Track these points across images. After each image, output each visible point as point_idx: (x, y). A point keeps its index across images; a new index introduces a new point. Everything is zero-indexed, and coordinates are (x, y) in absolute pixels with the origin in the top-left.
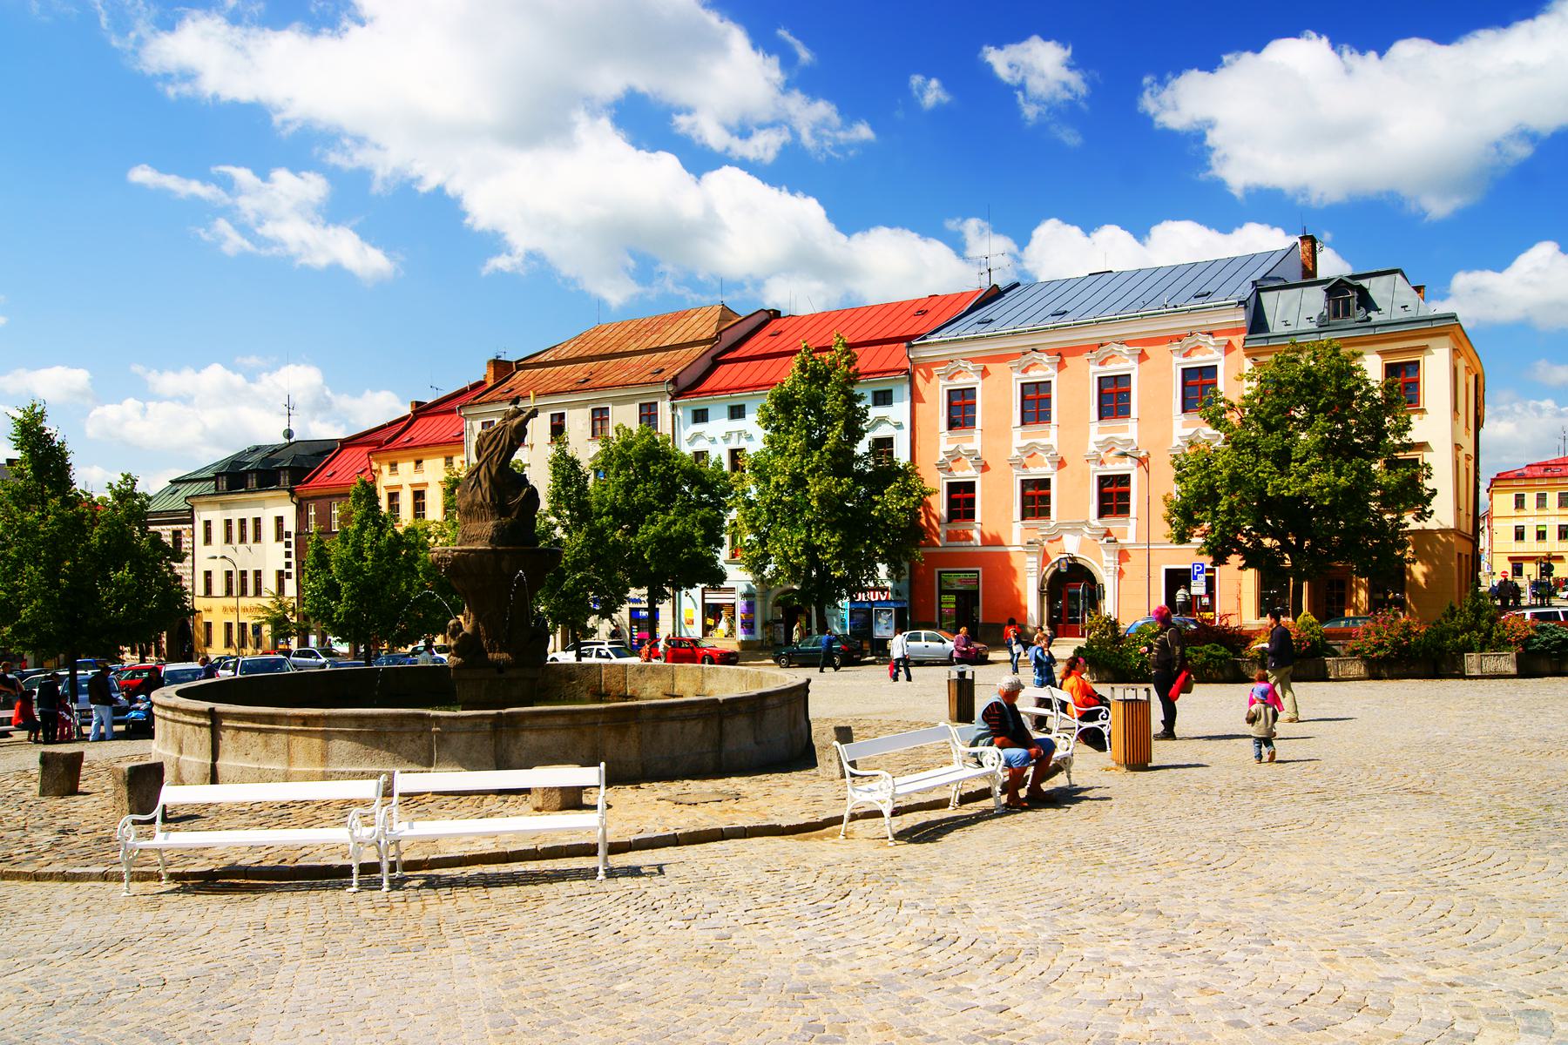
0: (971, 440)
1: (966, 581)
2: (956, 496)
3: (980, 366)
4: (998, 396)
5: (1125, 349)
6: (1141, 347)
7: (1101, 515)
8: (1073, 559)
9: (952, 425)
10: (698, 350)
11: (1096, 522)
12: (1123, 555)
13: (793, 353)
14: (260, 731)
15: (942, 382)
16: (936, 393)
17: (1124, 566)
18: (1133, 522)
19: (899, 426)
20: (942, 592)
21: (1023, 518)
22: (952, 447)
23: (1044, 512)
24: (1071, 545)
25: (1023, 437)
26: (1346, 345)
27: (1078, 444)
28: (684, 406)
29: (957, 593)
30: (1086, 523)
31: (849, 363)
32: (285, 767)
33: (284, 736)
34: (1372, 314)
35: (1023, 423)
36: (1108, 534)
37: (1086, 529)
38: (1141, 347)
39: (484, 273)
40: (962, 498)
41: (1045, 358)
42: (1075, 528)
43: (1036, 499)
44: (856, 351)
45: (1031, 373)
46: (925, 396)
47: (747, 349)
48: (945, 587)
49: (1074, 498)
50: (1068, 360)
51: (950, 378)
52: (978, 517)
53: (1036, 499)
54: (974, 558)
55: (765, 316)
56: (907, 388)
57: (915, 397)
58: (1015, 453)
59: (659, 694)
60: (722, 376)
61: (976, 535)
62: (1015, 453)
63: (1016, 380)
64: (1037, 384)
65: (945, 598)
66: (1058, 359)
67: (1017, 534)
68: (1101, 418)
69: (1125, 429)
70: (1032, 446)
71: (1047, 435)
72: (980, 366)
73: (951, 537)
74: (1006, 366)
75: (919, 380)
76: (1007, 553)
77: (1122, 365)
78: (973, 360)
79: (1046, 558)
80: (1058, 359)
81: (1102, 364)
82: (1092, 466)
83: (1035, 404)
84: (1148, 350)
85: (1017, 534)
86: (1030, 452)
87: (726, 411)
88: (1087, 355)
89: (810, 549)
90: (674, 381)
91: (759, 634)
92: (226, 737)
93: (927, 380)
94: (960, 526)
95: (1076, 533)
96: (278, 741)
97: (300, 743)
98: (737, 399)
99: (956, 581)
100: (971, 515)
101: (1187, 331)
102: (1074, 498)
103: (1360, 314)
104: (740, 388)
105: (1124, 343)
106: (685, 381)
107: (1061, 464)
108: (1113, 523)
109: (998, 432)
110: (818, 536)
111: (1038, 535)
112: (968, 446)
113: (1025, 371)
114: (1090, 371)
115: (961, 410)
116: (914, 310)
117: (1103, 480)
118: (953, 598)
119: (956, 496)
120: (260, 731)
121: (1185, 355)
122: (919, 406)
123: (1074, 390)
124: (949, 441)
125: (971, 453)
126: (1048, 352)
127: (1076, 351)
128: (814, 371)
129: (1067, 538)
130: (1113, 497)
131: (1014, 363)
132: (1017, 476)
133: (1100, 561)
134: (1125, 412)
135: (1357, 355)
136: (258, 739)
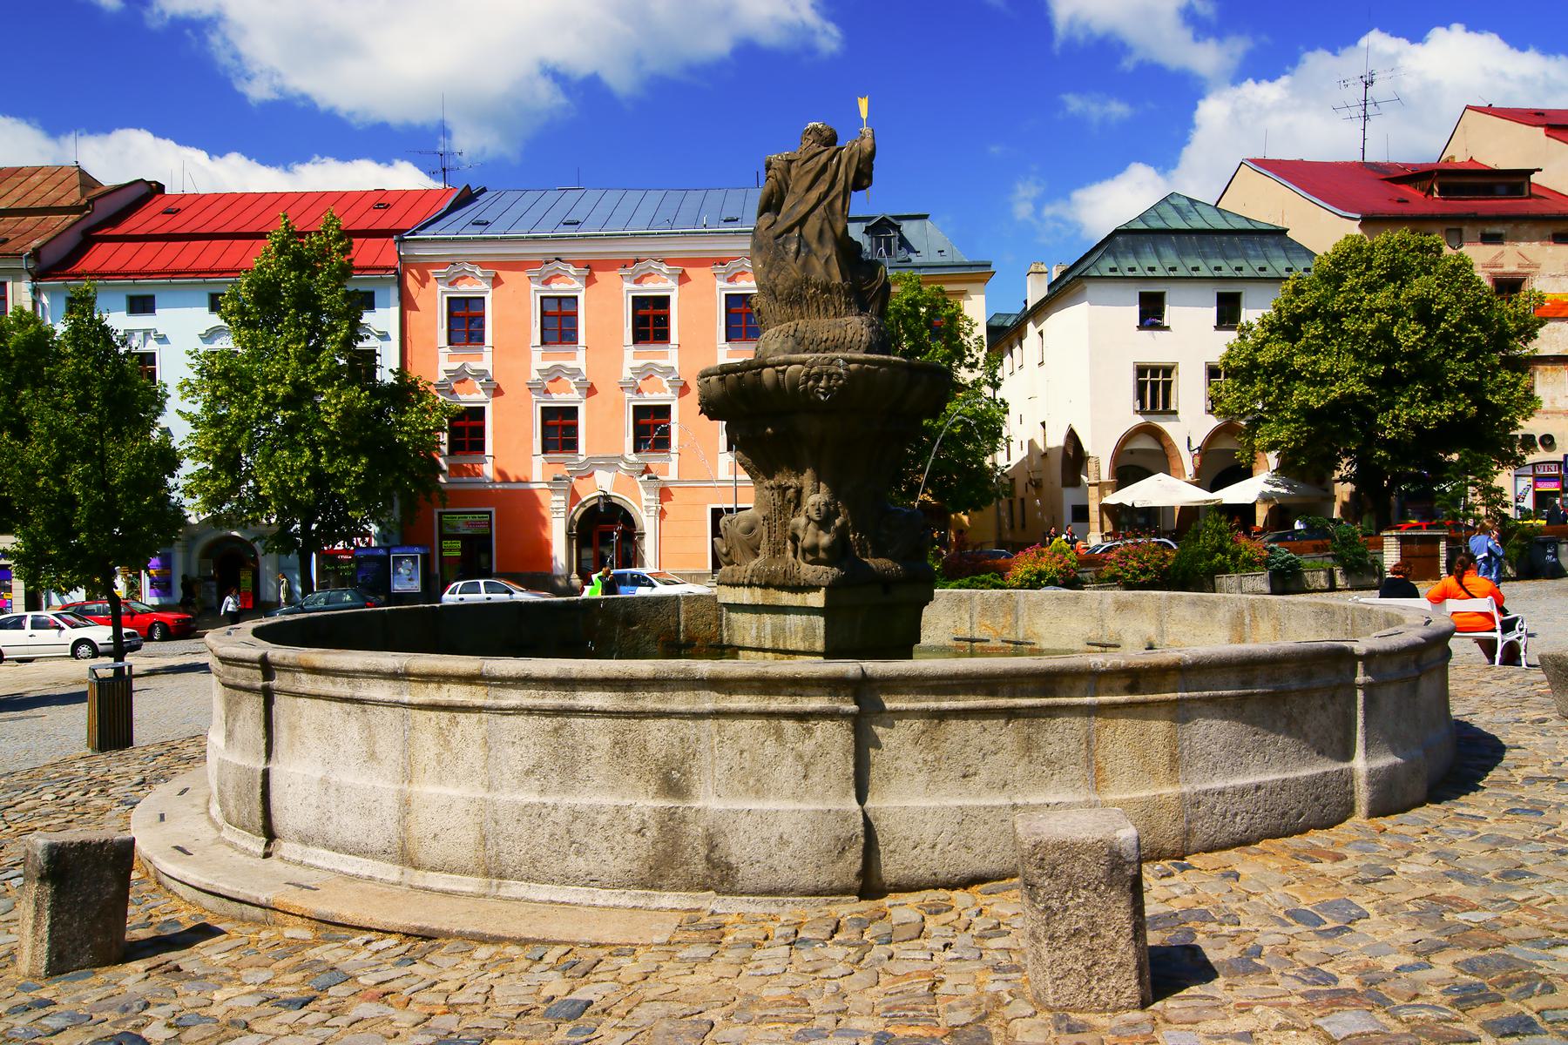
0: (665, 356)
1: (474, 524)
2: (550, 422)
3: (491, 272)
4: (513, 308)
5: (664, 268)
6: (590, 270)
7: (637, 450)
8: (607, 497)
9: (640, 336)
10: (58, 222)
11: (633, 458)
12: (665, 494)
13: (260, 236)
14: (1011, 714)
15: (441, 288)
16: (434, 300)
17: (666, 505)
18: (675, 458)
19: (384, 336)
20: (443, 537)
21: (544, 451)
22: (456, 365)
23: (570, 445)
24: (604, 482)
25: (544, 358)
26: (928, 283)
27: (610, 371)
28: (52, 292)
29: (465, 539)
30: (622, 458)
31: (345, 251)
32: (481, 793)
33: (1078, 722)
34: (912, 256)
35: (543, 343)
36: (647, 470)
37: (623, 465)
38: (683, 268)
39: (1057, 53)
40: (468, 430)
41: (572, 270)
42: (610, 463)
43: (559, 429)
44: (357, 241)
45: (554, 286)
46: (419, 302)
47: (131, 225)
48: (447, 531)
49: (605, 429)
50: (598, 275)
51: (452, 284)
52: (489, 449)
53: (559, 429)
54: (484, 496)
55: (146, 189)
56: (394, 292)
57: (406, 303)
58: (535, 376)
59: (1079, 645)
60: (99, 256)
61: (488, 470)
62: (535, 376)
63: (534, 292)
64: (560, 298)
65: (447, 544)
66: (587, 272)
67: (537, 469)
68: (635, 341)
69: (665, 356)
70: (558, 368)
71: (574, 358)
72: (491, 272)
73: (456, 469)
74: (523, 275)
75: (411, 283)
76: (531, 491)
77: (661, 285)
78: (482, 265)
79: (574, 497)
80: (587, 272)
81: (638, 281)
82: (628, 395)
83: (559, 323)
84: (503, 274)
85: (537, 469)
86: (647, 373)
87: (124, 303)
88: (621, 272)
89: (319, 480)
90: (36, 254)
91: (178, 594)
92: (894, 740)
93: (423, 282)
94: (466, 461)
95: (608, 469)
96: (1062, 735)
97: (1119, 736)
98: (143, 287)
99: (462, 524)
100: (479, 447)
101: (633, 257)
102: (605, 429)
103: (902, 255)
104: (149, 274)
105: (663, 261)
106: (49, 257)
107: (591, 391)
108: (654, 460)
109: (512, 350)
110: (330, 462)
111: (562, 471)
112: (476, 365)
113: (547, 283)
114: (622, 291)
115: (466, 322)
116: (369, 202)
117: (639, 411)
118: (459, 544)
119: (550, 422)
120: (1011, 714)
121: (730, 280)
122: (411, 314)
123: (605, 308)
124: (636, 356)
125: (481, 374)
126: (575, 264)
127: (609, 265)
128: (298, 255)
129: (599, 474)
130: (651, 427)
131: (535, 272)
132: (631, 400)
133: (638, 500)
134: (573, 340)
135: (962, 294)
136: (1006, 734)
